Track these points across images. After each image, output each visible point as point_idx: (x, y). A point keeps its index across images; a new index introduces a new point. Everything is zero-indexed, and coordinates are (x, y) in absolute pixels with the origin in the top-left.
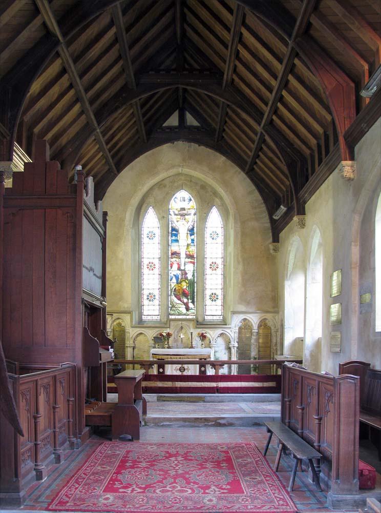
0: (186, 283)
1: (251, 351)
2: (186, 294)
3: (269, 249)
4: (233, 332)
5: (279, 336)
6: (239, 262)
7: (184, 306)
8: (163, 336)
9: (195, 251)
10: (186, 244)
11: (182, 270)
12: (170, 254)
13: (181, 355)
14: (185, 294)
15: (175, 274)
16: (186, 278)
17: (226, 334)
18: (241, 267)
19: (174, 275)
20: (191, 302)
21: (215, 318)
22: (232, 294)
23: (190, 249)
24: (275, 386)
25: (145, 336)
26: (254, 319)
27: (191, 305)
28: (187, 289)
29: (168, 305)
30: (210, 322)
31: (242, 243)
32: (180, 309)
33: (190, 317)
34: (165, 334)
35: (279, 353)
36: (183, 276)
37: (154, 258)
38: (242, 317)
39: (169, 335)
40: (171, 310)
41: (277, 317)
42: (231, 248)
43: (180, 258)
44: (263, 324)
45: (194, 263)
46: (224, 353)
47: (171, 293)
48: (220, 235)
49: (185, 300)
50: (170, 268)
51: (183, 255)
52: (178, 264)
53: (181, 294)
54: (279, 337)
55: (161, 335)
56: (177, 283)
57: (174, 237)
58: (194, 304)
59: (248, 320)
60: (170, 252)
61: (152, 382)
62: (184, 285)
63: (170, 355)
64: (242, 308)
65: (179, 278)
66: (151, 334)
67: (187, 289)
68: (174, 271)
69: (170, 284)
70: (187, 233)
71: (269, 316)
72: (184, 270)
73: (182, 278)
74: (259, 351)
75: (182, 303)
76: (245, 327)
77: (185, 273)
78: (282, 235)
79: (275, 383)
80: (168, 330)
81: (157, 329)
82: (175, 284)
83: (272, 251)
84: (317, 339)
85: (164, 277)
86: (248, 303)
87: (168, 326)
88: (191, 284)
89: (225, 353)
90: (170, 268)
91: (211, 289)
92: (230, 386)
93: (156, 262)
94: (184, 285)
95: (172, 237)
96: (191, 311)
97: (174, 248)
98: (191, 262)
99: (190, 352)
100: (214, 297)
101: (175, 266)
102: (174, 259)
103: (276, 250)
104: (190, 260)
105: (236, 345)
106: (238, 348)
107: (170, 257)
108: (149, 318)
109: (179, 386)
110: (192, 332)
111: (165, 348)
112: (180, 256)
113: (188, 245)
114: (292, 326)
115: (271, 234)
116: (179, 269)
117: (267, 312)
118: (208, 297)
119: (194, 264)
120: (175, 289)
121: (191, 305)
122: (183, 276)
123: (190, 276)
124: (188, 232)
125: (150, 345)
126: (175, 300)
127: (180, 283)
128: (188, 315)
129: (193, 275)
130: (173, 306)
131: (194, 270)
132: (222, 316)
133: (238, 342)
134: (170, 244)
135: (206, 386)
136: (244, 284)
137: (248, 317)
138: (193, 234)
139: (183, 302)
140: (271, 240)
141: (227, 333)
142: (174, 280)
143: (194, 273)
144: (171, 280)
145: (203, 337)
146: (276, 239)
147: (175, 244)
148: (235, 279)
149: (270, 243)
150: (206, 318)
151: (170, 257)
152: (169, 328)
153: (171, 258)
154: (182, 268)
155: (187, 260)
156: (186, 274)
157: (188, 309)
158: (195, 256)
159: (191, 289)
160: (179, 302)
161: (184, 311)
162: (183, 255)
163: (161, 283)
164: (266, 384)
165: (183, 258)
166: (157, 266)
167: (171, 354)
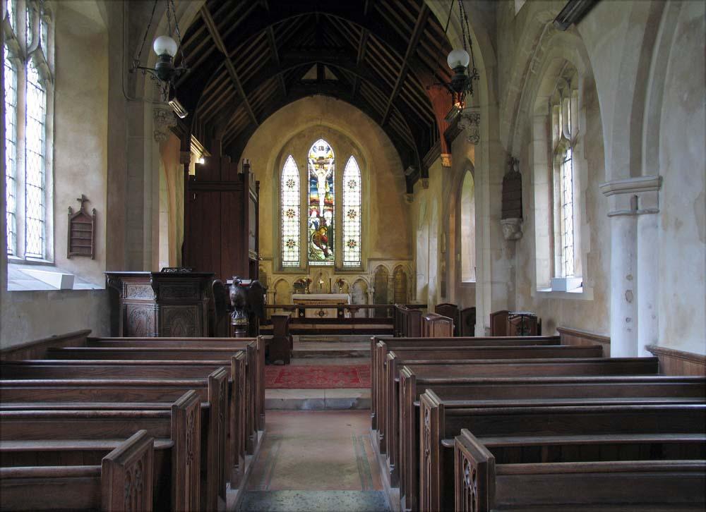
4: (369, 278)
7: (323, 253)
12: (309, 178)
14: (324, 241)
18: (377, 216)
21: (353, 264)
23: (329, 198)
26: (390, 266)
27: (330, 252)
32: (320, 255)
34: (305, 281)
39: (309, 281)
42: (368, 197)
44: (398, 269)
48: (358, 184)
49: (324, 247)
51: (322, 203)
53: (319, 240)
55: (302, 281)
58: (332, 251)
64: (379, 255)
66: (292, 280)
68: (313, 218)
71: (404, 263)
74: (395, 296)
76: (381, 271)
77: (323, 220)
80: (308, 277)
81: (298, 275)
83: (407, 202)
86: (384, 250)
88: (330, 231)
95: (311, 185)
97: (314, 196)
98: (329, 210)
100: (352, 244)
101: (314, 214)
102: (313, 207)
103: (410, 200)
104: (328, 208)
105: (373, 290)
106: (374, 293)
108: (289, 264)
113: (327, 193)
117: (402, 259)
118: (346, 244)
121: (330, 252)
123: (328, 223)
126: (315, 246)
127: (320, 230)
129: (332, 223)
137: (384, 263)
139: (322, 248)
140: (405, 191)
142: (313, 227)
143: (332, 220)
145: (341, 283)
147: (315, 192)
155: (326, 208)
157: (326, 255)
160: (318, 248)
162: (322, 203)
163: (301, 230)
165: (322, 207)
166: (297, 213)
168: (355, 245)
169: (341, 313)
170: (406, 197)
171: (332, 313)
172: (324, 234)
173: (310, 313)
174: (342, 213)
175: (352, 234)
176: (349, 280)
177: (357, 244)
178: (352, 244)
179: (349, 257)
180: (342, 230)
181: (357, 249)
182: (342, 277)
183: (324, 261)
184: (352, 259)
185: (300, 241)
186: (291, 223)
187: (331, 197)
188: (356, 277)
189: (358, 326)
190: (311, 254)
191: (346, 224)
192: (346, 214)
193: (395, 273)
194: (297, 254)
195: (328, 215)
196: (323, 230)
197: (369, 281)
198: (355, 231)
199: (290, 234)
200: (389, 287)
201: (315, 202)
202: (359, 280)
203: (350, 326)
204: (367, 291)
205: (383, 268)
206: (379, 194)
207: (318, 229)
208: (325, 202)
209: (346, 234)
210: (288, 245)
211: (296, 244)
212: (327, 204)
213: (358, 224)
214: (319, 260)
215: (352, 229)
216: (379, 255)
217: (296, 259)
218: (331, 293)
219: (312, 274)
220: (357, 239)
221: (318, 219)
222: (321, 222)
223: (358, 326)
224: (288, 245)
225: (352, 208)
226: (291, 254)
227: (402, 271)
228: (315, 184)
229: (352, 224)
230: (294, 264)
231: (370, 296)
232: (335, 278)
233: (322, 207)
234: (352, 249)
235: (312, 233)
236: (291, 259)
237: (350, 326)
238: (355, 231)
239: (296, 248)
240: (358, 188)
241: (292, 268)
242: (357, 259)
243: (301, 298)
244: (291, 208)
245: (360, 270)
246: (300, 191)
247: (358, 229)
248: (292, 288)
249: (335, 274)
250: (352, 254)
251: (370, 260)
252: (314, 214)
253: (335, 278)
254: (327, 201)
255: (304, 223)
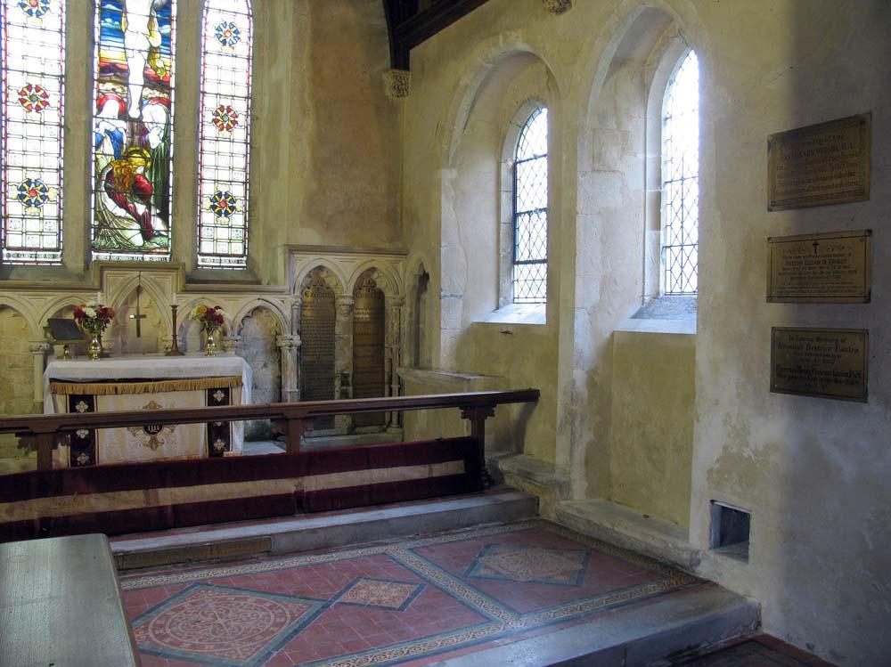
0: (145, 158)
1: (333, 356)
2: (142, 189)
3: (381, 86)
4: (285, 306)
5: (407, 315)
6: (304, 112)
7: (137, 226)
8: (85, 316)
9: (173, 70)
10: (146, 47)
11: (131, 120)
12: (96, 69)
13: (150, 380)
14: (140, 192)
15: (113, 129)
16: (146, 145)
17: (268, 310)
18: (310, 124)
19: (107, 132)
20: (159, 215)
21: (225, 262)
22: (288, 192)
23: (159, 64)
24: (462, 471)
25: (17, 314)
26: (344, 271)
27: (157, 224)
28: (147, 175)
29: (90, 221)
30: (216, 273)
31: (314, 58)
32: (128, 234)
33: (156, 258)
34: (91, 313)
35: (406, 360)
36: (137, 137)
37: (43, 74)
38: (311, 261)
39: (104, 314)
40: (96, 235)
41: (400, 267)
42: (284, 69)
43: (127, 85)
44: (368, 287)
45: (168, 104)
46: (262, 364)
47: (98, 184)
48: (244, 36)
49: (141, 209)
50: (95, 111)
51: (136, 77)
52: (121, 101)
53: (126, 188)
54: (407, 319)
55: (80, 314)
56: (117, 155)
57: (109, 20)
58: (166, 221)
59: (328, 271)
60: (96, 61)
61: (68, 498)
62: (139, 166)
63: (113, 381)
64: (311, 237)
65: (122, 143)
66: (38, 309)
67: (147, 175)
68: (108, 119)
69: (94, 158)
70: (151, 17)
71: (381, 262)
72: (140, 120)
73: (132, 144)
74: (355, 356)
75: (128, 215)
76: (319, 286)
77: (139, 129)
78: (421, 52)
79: (461, 462)
80: (100, 299)
81: (61, 295)
82: (109, 159)
83: (389, 92)
84: (607, 335)
85: (76, 133)
86: (327, 225)
87: (97, 284)
88: (159, 162)
89: (265, 365)
90: (95, 111)
91: (216, 181)
92: (339, 486)
93: (52, 86)
94: (139, 166)
95: (102, 18)
96: (158, 240)
97: (110, 52)
98: (160, 100)
99: (179, 370)
100: (223, 205)
101: (112, 108)
102: (109, 86)
103: (401, 90)
104: (157, 94)
105: (297, 340)
106: (300, 349)
107: (96, 77)
108: (26, 257)
109: (169, 503)
110: (174, 303)
111: (90, 356)
112: (127, 78)
113: (152, 51)
114: (461, 293)
115: (387, 47)
116: (123, 114)
117: (379, 252)
118: (207, 203)
119: (169, 106)
120: (111, 171)
121: (157, 224)
122: (137, 137)
123: (155, 140)
124: (154, 14)
125: (35, 345)
126: (111, 205)
127: (128, 156)
128: (149, 252)
129: (166, 138)
130: (103, 224)
131: (168, 124)
132: (245, 259)
133: (299, 333)
134: (97, 39)
135: (265, 493)
136: (320, 167)
137: (329, 261)
138: (169, 22)
139: (135, 214)
140: (387, 62)
141: (273, 308)
142: (108, 147)
143: (167, 132)
144: (97, 147)
145: (211, 319)
146: (400, 61)
147: (112, 42)
148: (295, 150)
149: (386, 71)
150: (200, 263)
151: (96, 77)
152: (101, 288)
153: (100, 81)
154: (134, 113)
155: (148, 92)
156: (145, 132)
157: (147, 233)
158: (173, 84)
159: (159, 179)
160: (121, 212)
161: (138, 240)
162: (136, 77)
163: (67, 151)
164: (439, 470)
165: (136, 90)
166: (54, 100)
167: (116, 377)
168: (233, 208)
169: (219, 444)
170: (388, 80)
171: (187, 442)
172: (140, 171)
173: (116, 446)
174: (197, 112)
175: (224, 175)
176: (232, 308)
177: (239, 205)
178: (223, 205)
179: (215, 240)
180: (197, 164)
181: (238, 219)
182: (211, 301)
183: (139, 250)
184: (223, 248)
185: (65, 187)
186: (33, 130)
187: (166, 62)
188: (250, 301)
189: (316, 483)
190: (98, 229)
191: (207, 145)
192: (209, 117)
193: (358, 288)
194: (54, 226)
195: (155, 115)
196: (137, 160)
197: (287, 313)
198: (231, 169)
199: (32, 161)
200: (338, 329)
201: (115, 72)
202: (258, 309)
203: (287, 486)
204: (282, 343)
205: (323, 275)
206: (317, 70)
207: (121, 155)
208: (146, 76)
209: (206, 174)
210: (21, 197)
211: (52, 194)
212: (154, 82)
213: (241, 149)
214: (126, 247)
215: (224, 161)
216: (311, 237)
217: (51, 242)
218: (176, 351)
219: (111, 289)
220: (238, 191)
221: (123, 125)
222: (133, 134)
223: (316, 483)
224: (21, 197)
225: (226, 103)
226: (33, 225)
227: (372, 284)
228: (117, 16)
229: (224, 147)
230: (42, 257)
231: (290, 358)
232: (190, 305)
233: (136, 90)
234: (223, 219)
235: (103, 163)
236: (33, 242)
237: (287, 486)
238: (217, 168)
239: (50, 210)
240: (243, 48)
241: (36, 268)
242: (238, 248)
243: (81, 375)
244: (34, 81)
245: (246, 279)
246: (68, 31)
247: (240, 162)
248: (38, 336)
249: (186, 291)
250: (223, 233)
251: (292, 250)
252: (112, 108)
253: (190, 305)
254: (152, 72)
255: (81, 133)
